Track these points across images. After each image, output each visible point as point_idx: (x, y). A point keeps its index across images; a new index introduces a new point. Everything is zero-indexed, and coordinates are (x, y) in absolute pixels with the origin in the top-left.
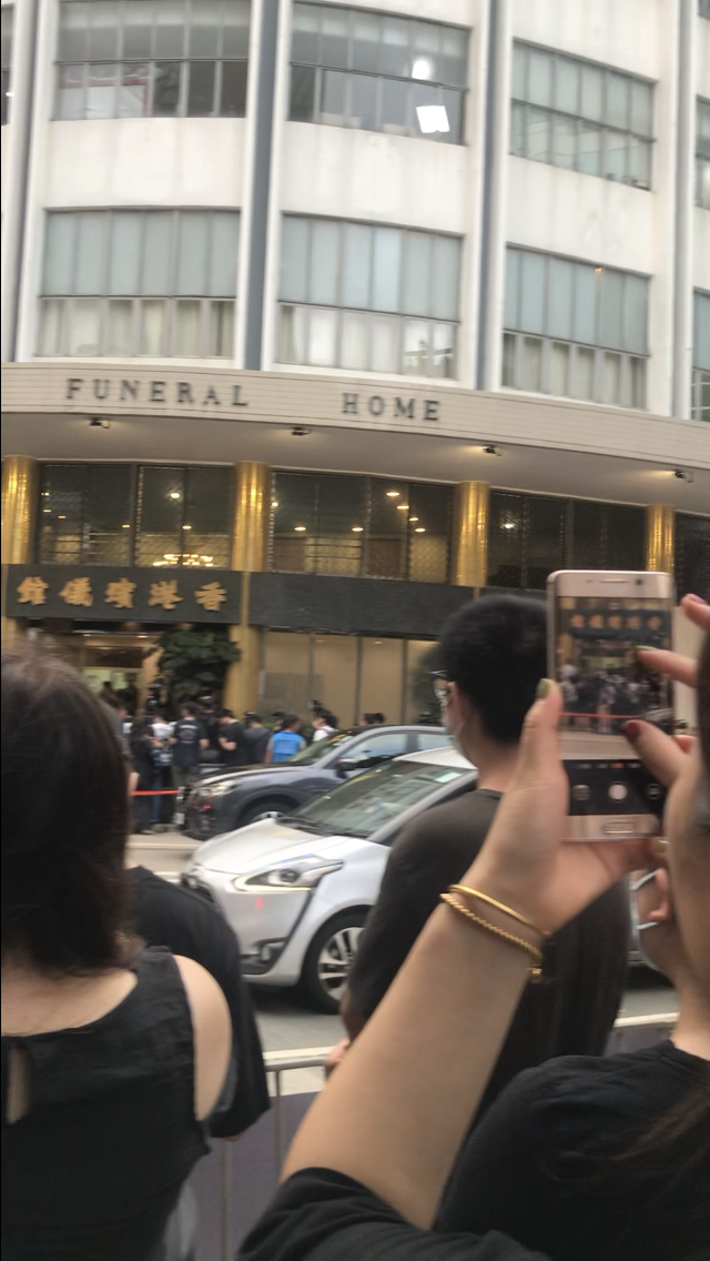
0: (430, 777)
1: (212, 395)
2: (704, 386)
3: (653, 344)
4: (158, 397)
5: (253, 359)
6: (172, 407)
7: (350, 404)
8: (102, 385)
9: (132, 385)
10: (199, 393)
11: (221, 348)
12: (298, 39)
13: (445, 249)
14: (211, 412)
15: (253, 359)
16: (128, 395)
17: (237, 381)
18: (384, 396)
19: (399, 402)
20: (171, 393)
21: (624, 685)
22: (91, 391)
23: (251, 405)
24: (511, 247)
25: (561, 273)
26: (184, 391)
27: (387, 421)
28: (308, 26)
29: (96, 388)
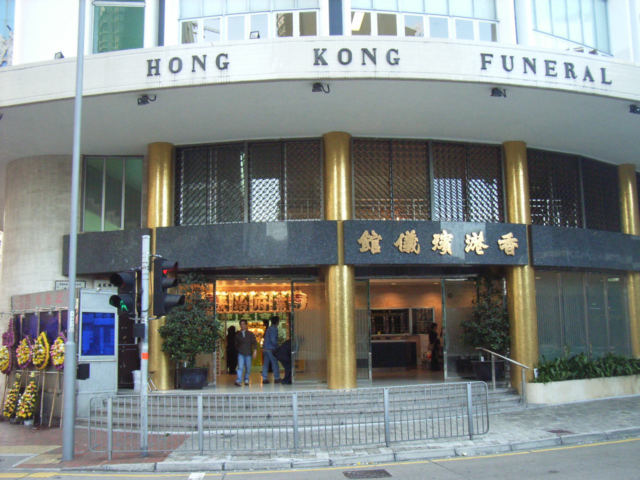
8: (508, 61)
20: (560, 70)
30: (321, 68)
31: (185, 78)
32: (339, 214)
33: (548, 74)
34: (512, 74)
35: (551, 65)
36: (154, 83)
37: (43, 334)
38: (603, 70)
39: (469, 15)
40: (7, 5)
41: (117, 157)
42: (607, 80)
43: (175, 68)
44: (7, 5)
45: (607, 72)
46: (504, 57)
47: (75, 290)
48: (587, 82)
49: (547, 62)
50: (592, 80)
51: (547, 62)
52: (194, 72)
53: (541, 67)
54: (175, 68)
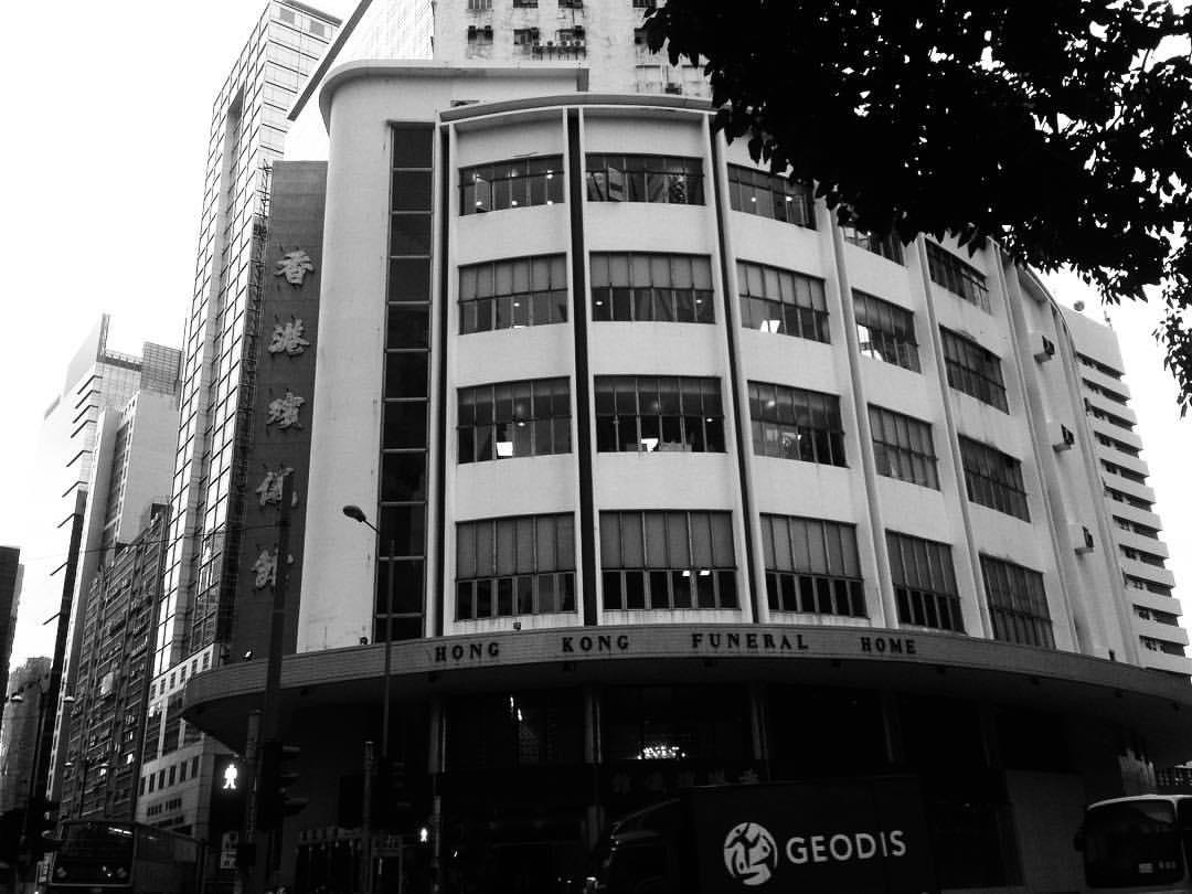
0: (199, 772)
1: (785, 642)
2: (275, 614)
3: (865, 573)
4: (752, 644)
5: (590, 618)
6: (762, 651)
7: (696, 639)
8: (715, 638)
9: (606, 639)
10: (778, 642)
11: (569, 606)
12: (753, 403)
13: (717, 523)
14: (786, 653)
15: (590, 618)
16: (733, 644)
17: (583, 634)
18: (590, 636)
19: (892, 641)
20: (760, 641)
21: (615, 846)
22: (709, 642)
23: (810, 646)
24: (762, 515)
25: (797, 528)
26: (768, 640)
27: (888, 654)
28: (755, 396)
29: (712, 640)
30: (569, 653)
31: (465, 662)
32: (596, 758)
33: (749, 646)
34: (720, 650)
35: (752, 638)
36: (441, 666)
37: (210, 649)
38: (800, 637)
39: (790, 569)
40: (477, 281)
41: (1037, 448)
42: (804, 644)
43: (458, 654)
44: (477, 281)
45: (803, 639)
46: (712, 636)
47: (189, 746)
48: (786, 649)
49: (749, 636)
50: (789, 647)
51: (749, 636)
52: (1083, 307)
53: (743, 640)
54: (458, 654)
